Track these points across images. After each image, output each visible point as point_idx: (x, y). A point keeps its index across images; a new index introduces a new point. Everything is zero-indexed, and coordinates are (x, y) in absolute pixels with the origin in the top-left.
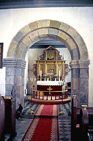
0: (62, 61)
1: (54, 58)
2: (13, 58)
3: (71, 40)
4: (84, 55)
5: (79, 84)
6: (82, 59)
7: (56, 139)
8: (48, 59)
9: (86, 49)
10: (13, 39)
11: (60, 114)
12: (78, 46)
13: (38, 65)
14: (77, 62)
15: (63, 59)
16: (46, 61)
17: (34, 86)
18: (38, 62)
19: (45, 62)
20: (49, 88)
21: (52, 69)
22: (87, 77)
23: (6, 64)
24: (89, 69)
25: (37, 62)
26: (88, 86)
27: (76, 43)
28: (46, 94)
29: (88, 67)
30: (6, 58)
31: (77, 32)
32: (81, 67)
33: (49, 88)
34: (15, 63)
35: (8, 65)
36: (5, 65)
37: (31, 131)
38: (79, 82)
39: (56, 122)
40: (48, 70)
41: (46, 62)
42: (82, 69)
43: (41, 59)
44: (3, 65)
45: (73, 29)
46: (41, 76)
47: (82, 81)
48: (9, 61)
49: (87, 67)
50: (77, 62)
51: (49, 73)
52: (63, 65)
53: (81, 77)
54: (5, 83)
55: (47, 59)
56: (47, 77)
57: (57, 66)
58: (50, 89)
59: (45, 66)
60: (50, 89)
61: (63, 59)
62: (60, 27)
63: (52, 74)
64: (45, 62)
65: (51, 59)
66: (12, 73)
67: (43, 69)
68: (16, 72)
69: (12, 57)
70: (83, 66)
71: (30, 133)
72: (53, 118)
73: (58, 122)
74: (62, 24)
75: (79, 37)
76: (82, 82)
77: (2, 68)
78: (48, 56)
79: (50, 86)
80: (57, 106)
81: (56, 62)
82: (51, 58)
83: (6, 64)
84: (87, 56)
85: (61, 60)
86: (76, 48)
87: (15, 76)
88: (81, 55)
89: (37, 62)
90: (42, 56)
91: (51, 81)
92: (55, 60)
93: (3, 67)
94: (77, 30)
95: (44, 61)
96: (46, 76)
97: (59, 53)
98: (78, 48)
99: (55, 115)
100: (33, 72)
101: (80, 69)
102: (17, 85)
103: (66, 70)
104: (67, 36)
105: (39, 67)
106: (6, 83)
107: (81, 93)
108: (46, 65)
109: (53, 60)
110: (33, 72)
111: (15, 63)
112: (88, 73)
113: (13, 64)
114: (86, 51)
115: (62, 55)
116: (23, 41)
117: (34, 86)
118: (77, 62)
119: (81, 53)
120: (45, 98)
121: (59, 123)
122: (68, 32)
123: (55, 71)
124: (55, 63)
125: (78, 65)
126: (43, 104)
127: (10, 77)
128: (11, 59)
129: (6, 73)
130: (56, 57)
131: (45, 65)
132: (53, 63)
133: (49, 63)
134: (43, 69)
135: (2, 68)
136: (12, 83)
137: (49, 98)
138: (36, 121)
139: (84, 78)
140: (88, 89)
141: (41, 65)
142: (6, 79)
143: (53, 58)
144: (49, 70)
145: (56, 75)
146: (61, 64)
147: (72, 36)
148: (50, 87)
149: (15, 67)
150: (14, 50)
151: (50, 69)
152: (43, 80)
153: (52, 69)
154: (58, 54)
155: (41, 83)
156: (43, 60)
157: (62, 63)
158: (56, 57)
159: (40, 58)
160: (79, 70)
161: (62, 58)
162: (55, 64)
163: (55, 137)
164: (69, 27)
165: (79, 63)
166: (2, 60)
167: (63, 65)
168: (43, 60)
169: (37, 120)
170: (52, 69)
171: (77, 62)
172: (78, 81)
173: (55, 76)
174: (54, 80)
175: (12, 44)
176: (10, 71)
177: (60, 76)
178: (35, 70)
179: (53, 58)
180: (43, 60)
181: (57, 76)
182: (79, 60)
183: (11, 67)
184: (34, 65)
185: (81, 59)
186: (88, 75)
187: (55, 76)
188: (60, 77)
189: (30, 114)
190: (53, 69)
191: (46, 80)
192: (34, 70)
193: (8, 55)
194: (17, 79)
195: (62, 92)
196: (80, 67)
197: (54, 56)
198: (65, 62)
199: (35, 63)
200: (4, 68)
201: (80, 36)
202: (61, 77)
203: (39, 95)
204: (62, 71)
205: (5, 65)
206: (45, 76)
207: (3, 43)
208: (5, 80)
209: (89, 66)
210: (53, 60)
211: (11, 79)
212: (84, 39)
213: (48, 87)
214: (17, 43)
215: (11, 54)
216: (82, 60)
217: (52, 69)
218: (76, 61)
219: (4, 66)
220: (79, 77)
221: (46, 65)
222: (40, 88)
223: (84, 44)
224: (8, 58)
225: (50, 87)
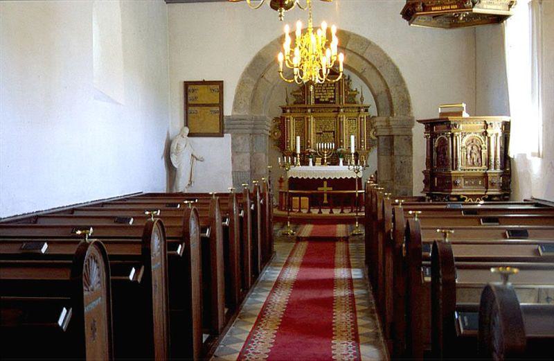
0: (359, 108)
1: (334, 99)
2: (247, 114)
3: (374, 73)
4: (402, 105)
5: (392, 170)
6: (397, 114)
7: (348, 354)
8: (317, 101)
9: (408, 94)
10: (244, 73)
11: (354, 235)
12: (389, 86)
13: (287, 119)
14: (388, 121)
15: (362, 102)
16: (311, 108)
17: (281, 181)
18: (288, 111)
19: (309, 111)
20: (322, 186)
21: (329, 132)
22: (410, 154)
23: (231, 126)
24: (412, 135)
25: (284, 111)
26: (412, 172)
27: (385, 81)
28: (316, 201)
29: (411, 131)
30: (230, 114)
31: (385, 55)
32: (395, 132)
33: (322, 186)
34: (251, 124)
35: (237, 129)
36: (229, 129)
37: (263, 337)
38: (393, 164)
39: (349, 331)
40: (317, 133)
41: (312, 112)
42: (399, 136)
43: (295, 103)
44: (225, 131)
45: (377, 48)
46: (298, 151)
47: (398, 160)
48: (240, 121)
49: (408, 133)
50: (386, 121)
51: (269, 128)
52: (361, 118)
53: (396, 152)
54: (230, 168)
55: (312, 102)
56: (316, 154)
57: (345, 121)
58: (325, 189)
59: (308, 121)
60: (325, 189)
61: (362, 99)
62: (348, 45)
63: (331, 146)
64: (309, 111)
65: (325, 102)
66: (247, 147)
67: (303, 132)
68: (253, 146)
69: (244, 113)
70: (400, 130)
71: (262, 342)
72: (337, 241)
73: (355, 319)
74: (351, 37)
75: (391, 66)
76: (398, 165)
77: (223, 136)
78: (317, 91)
79: (324, 179)
80: (346, 228)
81: (342, 110)
82: (327, 100)
83: (231, 126)
84: (409, 107)
85: (357, 105)
86: (383, 89)
87: (252, 154)
88: (395, 107)
89: (284, 110)
90: (298, 91)
91: (328, 165)
92: (337, 105)
93: (225, 135)
94: (387, 51)
95: (306, 108)
96: (313, 151)
97: (348, 83)
98: (388, 91)
99: (342, 236)
100: (275, 140)
101: (393, 136)
102: (257, 173)
103: (371, 133)
104: (364, 62)
105: (292, 124)
106: (233, 168)
107: (397, 188)
108: (312, 120)
109: (334, 105)
110: (275, 140)
111: (251, 124)
112: (411, 144)
113: (247, 126)
114: (406, 97)
115: (359, 90)
116: (266, 76)
117: (281, 179)
118: (386, 121)
119: (395, 101)
120: (315, 212)
121: (360, 322)
122: (366, 56)
123: (338, 138)
124: (338, 111)
125: (388, 126)
126: (311, 223)
127: (241, 156)
128: (243, 117)
129: (233, 147)
130: (340, 94)
131: (307, 118)
132: (334, 112)
133: (321, 115)
134: (303, 132)
135: (223, 136)
136: (247, 168)
137: (326, 212)
138: (257, 351)
139: (402, 156)
140: (411, 179)
141: (297, 119)
142: (233, 160)
143: (331, 99)
144: (320, 133)
145: (342, 149)
146: (355, 115)
147: (375, 63)
148: (325, 183)
149: (250, 134)
150: (250, 96)
151: (324, 132)
152: (304, 163)
153: (331, 132)
154: (348, 88)
155: (299, 171)
156: (302, 106)
157: (359, 111)
158: (340, 94)
159: (292, 100)
160: (391, 138)
161: (358, 98)
162: (339, 116)
163: (348, 349)
164: (369, 43)
165: (391, 123)
166: (223, 120)
167: (361, 118)
168: (302, 106)
169: (303, 246)
170: (329, 132)
171: (388, 121)
172: (390, 164)
173: (339, 150)
174: (337, 163)
175: (242, 83)
176: (241, 142)
177: (353, 151)
178: (278, 134)
179: (333, 97)
180: (301, 103)
181: (344, 150)
182: (391, 117)
183: (242, 134)
184: (276, 119)
185: (395, 114)
186: (412, 150)
187: (339, 150)
188: (353, 155)
189: (287, 234)
190: (334, 132)
191: (314, 165)
192: (276, 134)
193: (235, 108)
194: (258, 159)
195: (355, 193)
196: (393, 133)
197: (334, 92)
198: (366, 111)
199: (279, 113)
200: (228, 137)
201: (393, 64)
202: (356, 154)
203: (298, 207)
204: (361, 137)
205: (229, 129)
206: (310, 153)
207: (222, 82)
208: (231, 162)
209: (413, 129)
210: (334, 105)
211: (243, 159)
212: (401, 70)
213: (319, 182)
214: (255, 82)
215: (242, 106)
216: (398, 116)
217: (331, 132)
218: (384, 118)
219: (227, 133)
220: (392, 154)
221: (312, 120)
222: (296, 183)
223: (401, 81)
224: (235, 113)
225: (325, 183)
